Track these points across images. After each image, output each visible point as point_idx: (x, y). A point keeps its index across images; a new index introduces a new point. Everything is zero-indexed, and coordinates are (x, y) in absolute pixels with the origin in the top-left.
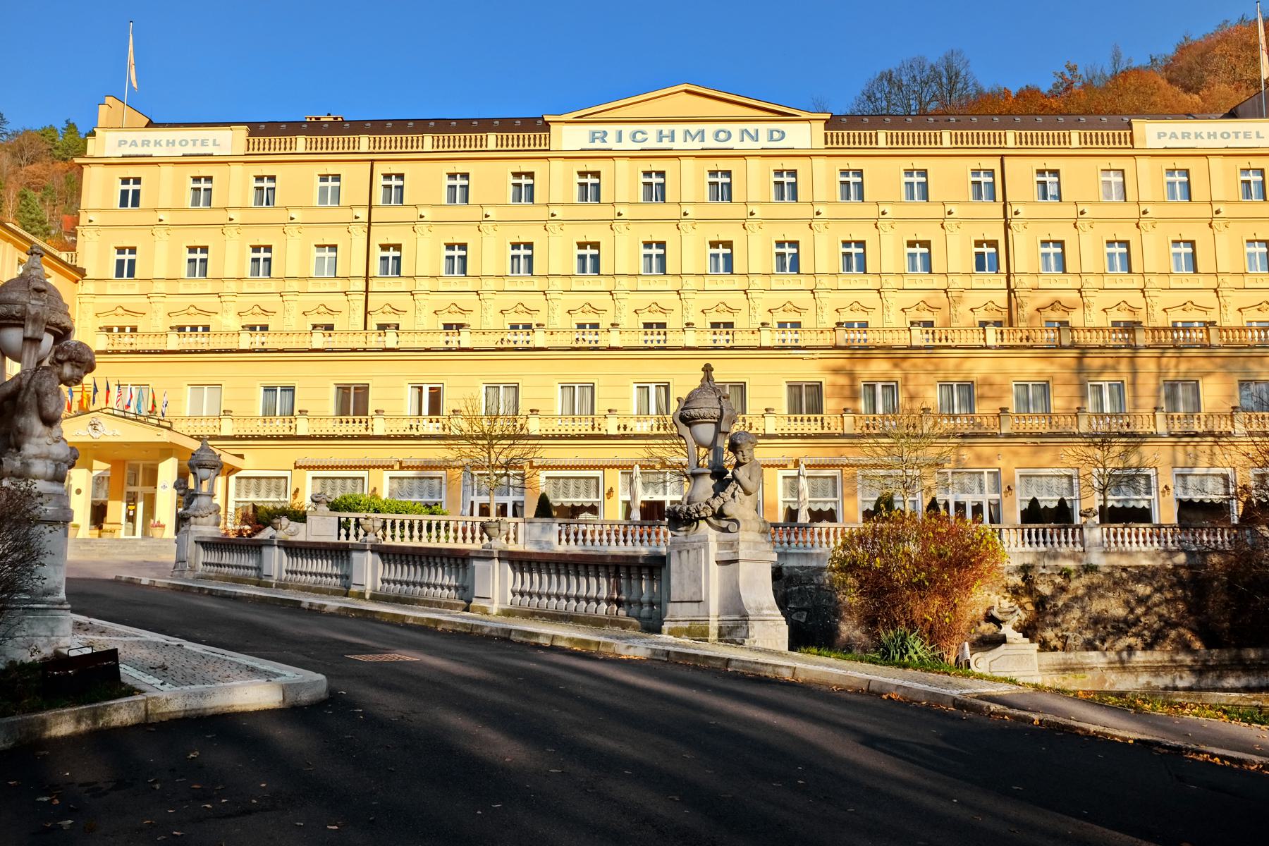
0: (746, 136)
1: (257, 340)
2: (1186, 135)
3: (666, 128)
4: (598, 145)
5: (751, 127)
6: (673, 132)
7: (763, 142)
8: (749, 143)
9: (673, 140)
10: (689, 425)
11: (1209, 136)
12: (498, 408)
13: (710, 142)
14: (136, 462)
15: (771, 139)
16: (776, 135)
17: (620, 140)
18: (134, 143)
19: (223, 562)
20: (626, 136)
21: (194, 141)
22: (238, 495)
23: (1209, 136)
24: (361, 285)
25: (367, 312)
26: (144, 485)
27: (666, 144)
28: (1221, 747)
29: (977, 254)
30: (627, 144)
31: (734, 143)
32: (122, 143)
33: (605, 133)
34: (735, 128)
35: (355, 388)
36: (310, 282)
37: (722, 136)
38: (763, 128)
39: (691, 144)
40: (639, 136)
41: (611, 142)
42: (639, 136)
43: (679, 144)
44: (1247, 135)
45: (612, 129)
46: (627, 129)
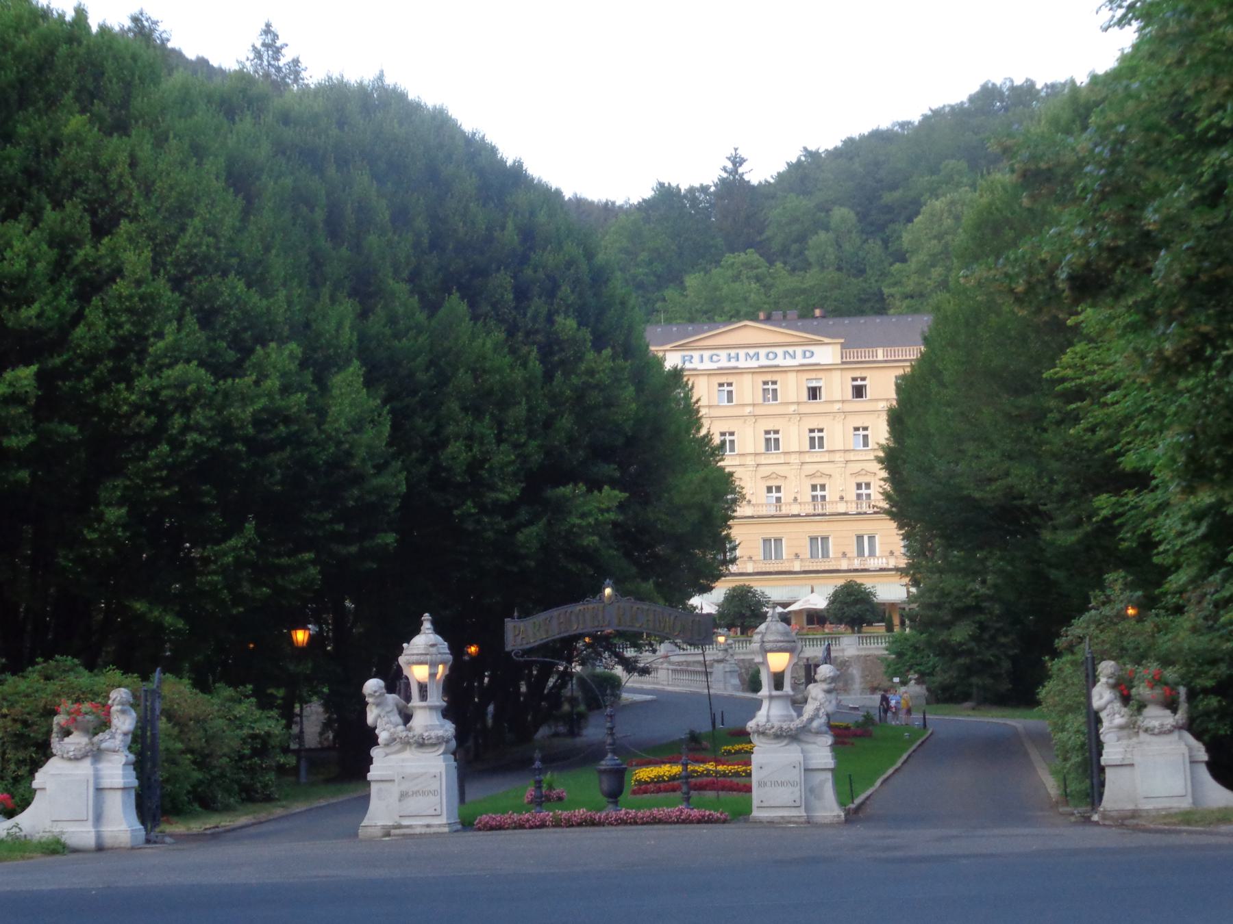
3: (733, 352)
5: (790, 350)
7: (799, 360)
8: (789, 362)
13: (763, 361)
15: (805, 357)
17: (702, 361)
27: (733, 363)
30: (707, 365)
31: (780, 361)
33: (692, 357)
34: (780, 351)
36: (852, 454)
37: (771, 356)
40: (715, 358)
43: (742, 363)
46: (707, 354)
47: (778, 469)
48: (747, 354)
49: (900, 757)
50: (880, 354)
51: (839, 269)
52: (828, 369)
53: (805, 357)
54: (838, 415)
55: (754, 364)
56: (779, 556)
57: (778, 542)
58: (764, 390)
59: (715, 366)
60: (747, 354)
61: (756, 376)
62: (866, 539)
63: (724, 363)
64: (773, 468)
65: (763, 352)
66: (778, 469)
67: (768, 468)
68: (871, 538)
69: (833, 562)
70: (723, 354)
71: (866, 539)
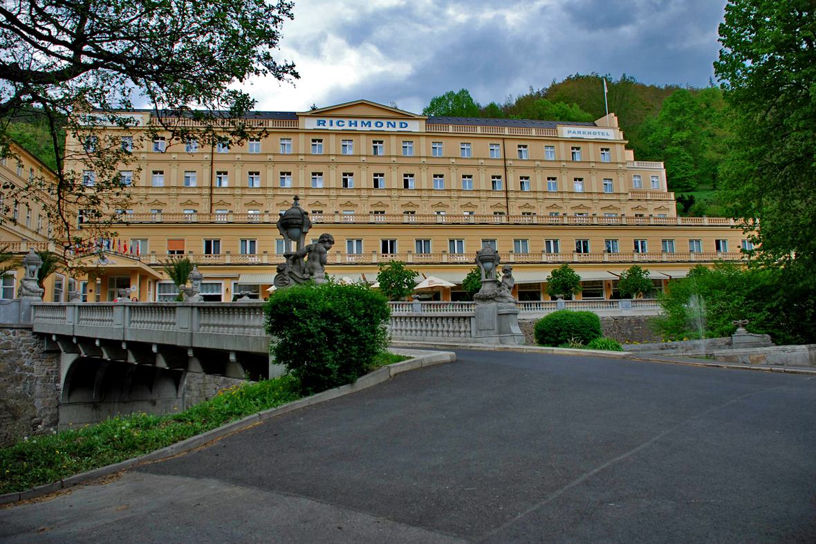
0: (390, 126)
1: (527, 220)
2: (579, 132)
4: (321, 127)
5: (392, 122)
6: (356, 122)
7: (398, 128)
8: (391, 129)
9: (356, 126)
10: (482, 263)
11: (588, 133)
12: (138, 251)
13: (373, 128)
14: (113, 277)
15: (401, 127)
16: (403, 125)
17: (332, 125)
18: (574, 132)
19: (246, 324)
20: (334, 123)
21: (599, 133)
22: (159, 292)
23: (588, 133)
24: (207, 191)
25: (212, 204)
26: (13, 285)
27: (353, 127)
28: (333, 402)
29: (404, 180)
30: (335, 127)
31: (384, 128)
32: (569, 132)
33: (325, 122)
34: (385, 122)
35: (214, 241)
36: (574, 194)
37: (379, 124)
38: (398, 123)
39: (364, 128)
40: (340, 123)
41: (327, 126)
42: (340, 123)
43: (359, 128)
44: (603, 134)
45: (328, 121)
46: (335, 121)
47: (614, 203)
48: (363, 122)
49: (127, 464)
50: (479, 130)
51: (635, 116)
52: (417, 135)
53: (401, 127)
54: (238, 163)
55: (367, 128)
56: (427, 251)
57: (427, 243)
58: (374, 147)
59: (340, 128)
60: (363, 122)
61: (369, 137)
62: (552, 242)
63: (347, 127)
64: (440, 200)
65: (373, 122)
66: (614, 203)
67: (575, 201)
68: (555, 242)
69: (432, 257)
70: (346, 122)
71: (552, 242)
